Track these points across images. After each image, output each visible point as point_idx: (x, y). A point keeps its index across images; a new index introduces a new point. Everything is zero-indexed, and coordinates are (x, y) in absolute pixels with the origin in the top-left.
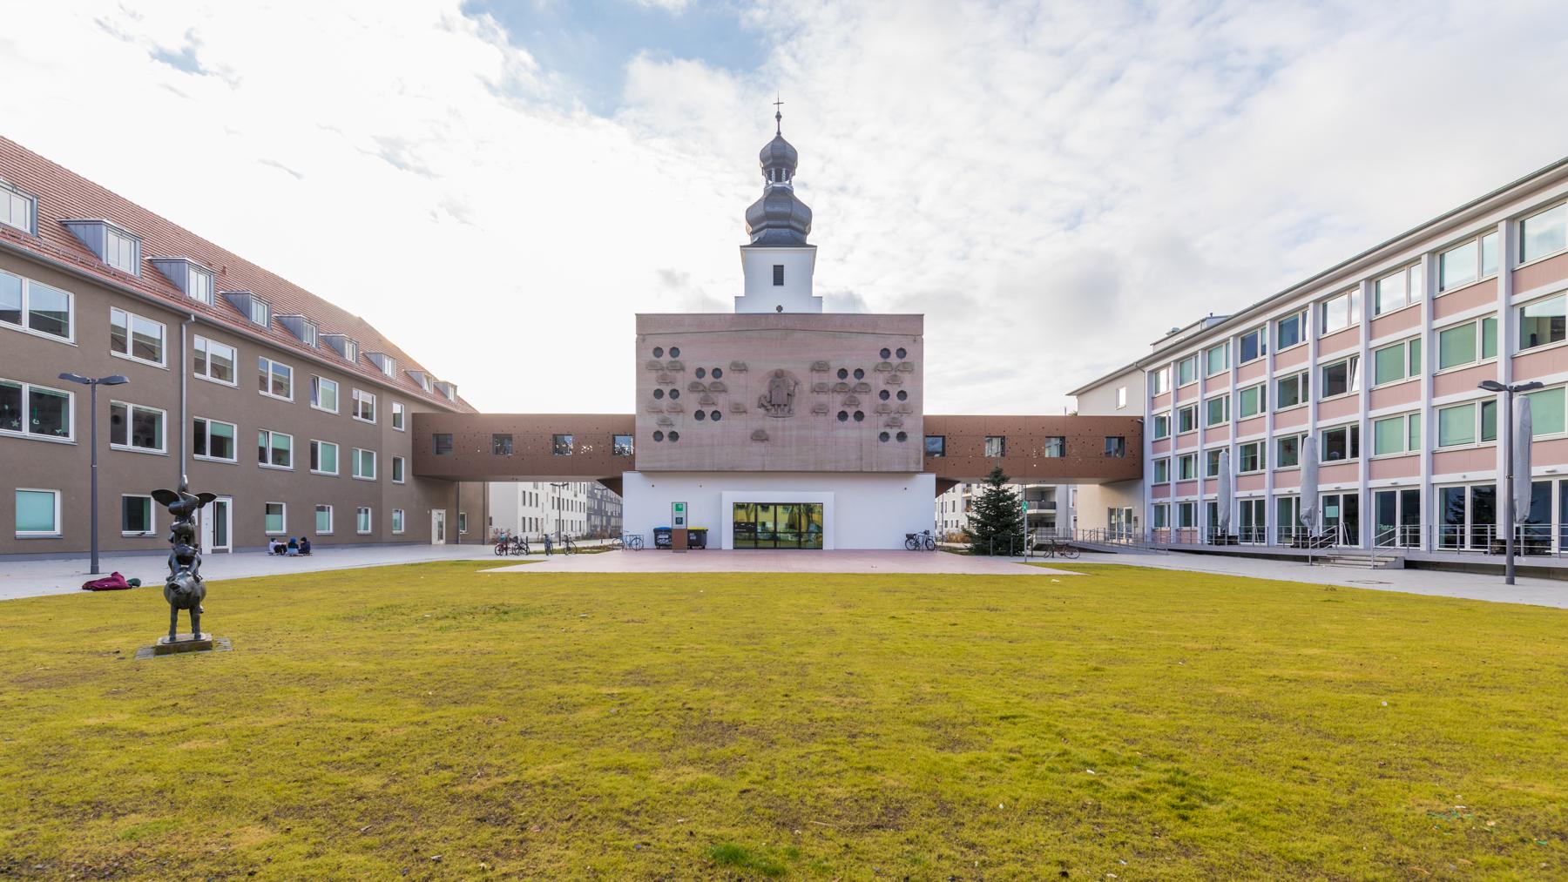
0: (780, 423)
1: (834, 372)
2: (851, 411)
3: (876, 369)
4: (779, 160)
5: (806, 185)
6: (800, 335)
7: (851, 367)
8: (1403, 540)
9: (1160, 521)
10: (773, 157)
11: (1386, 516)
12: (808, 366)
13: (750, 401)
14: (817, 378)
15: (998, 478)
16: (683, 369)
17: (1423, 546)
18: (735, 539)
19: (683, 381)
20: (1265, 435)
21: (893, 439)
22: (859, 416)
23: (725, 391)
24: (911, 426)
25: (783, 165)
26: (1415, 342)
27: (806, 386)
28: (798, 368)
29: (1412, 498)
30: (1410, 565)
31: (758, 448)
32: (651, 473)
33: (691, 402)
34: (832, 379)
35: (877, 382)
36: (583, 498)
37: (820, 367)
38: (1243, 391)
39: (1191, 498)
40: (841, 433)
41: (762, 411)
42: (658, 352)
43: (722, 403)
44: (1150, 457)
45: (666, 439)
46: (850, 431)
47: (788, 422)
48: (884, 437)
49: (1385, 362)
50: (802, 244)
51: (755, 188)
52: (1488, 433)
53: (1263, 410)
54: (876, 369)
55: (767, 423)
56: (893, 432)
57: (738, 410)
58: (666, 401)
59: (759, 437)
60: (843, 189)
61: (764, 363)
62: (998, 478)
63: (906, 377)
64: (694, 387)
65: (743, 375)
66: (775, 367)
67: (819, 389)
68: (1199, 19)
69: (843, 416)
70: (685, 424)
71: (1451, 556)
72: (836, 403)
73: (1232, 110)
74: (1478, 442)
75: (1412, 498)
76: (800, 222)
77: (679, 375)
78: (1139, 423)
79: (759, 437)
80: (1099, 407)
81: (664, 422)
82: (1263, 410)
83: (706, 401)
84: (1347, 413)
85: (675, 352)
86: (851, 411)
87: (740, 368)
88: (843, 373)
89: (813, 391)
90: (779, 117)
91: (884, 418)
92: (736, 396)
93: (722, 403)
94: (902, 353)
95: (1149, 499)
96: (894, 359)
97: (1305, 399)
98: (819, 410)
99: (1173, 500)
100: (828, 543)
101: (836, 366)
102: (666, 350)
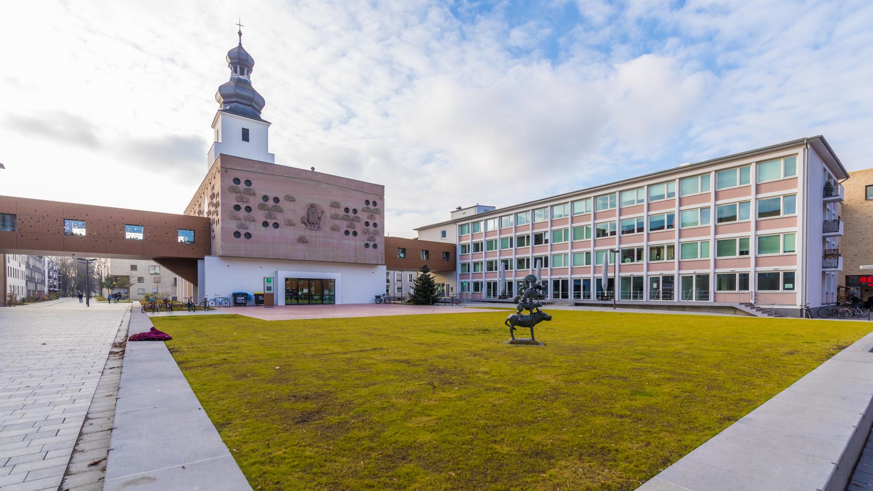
0: (314, 233)
1: (343, 209)
2: (351, 231)
3: (363, 210)
4: (240, 61)
5: (258, 81)
6: (325, 186)
7: (271, 195)
8: (584, 296)
9: (463, 289)
10: (239, 58)
11: (577, 288)
12: (329, 204)
13: (297, 220)
14: (334, 211)
15: (425, 269)
16: (254, 194)
17: (645, 300)
18: (286, 299)
19: (254, 202)
20: (512, 257)
21: (371, 247)
22: (355, 234)
23: (282, 211)
24: (378, 240)
25: (246, 66)
26: (566, 230)
27: (328, 215)
28: (323, 204)
29: (565, 282)
30: (577, 305)
31: (300, 247)
32: (224, 257)
33: (260, 216)
34: (342, 212)
35: (364, 217)
36: (23, 268)
37: (335, 205)
38: (502, 239)
39: (479, 280)
40: (346, 242)
41: (303, 225)
42: (237, 181)
43: (280, 218)
44: (459, 262)
45: (242, 236)
46: (350, 241)
47: (318, 233)
48: (367, 245)
49: (556, 235)
50: (258, 118)
51: (225, 75)
52: (588, 263)
53: (511, 246)
54: (363, 210)
55: (307, 233)
56: (371, 244)
57: (290, 223)
58: (242, 213)
59: (302, 240)
60: (172, 61)
61: (305, 199)
62: (425, 269)
63: (377, 216)
64: (262, 207)
65: (292, 203)
66: (311, 201)
67: (335, 217)
68: (381, 40)
69: (347, 233)
70: (255, 229)
71: (654, 302)
72: (344, 225)
73: (397, 92)
74: (585, 265)
75: (565, 282)
76: (258, 104)
77: (252, 198)
78: (454, 247)
79: (302, 240)
80: (434, 237)
81: (242, 226)
82: (511, 246)
83: (269, 216)
84: (544, 251)
85: (248, 183)
86: (351, 231)
87: (290, 199)
88: (347, 210)
89: (332, 217)
90: (240, 34)
91: (367, 236)
92: (289, 216)
93: (280, 218)
94: (375, 203)
95: (459, 280)
96: (371, 206)
97: (528, 244)
98: (335, 229)
99: (471, 280)
100: (338, 301)
101: (344, 205)
102: (371, 202)
